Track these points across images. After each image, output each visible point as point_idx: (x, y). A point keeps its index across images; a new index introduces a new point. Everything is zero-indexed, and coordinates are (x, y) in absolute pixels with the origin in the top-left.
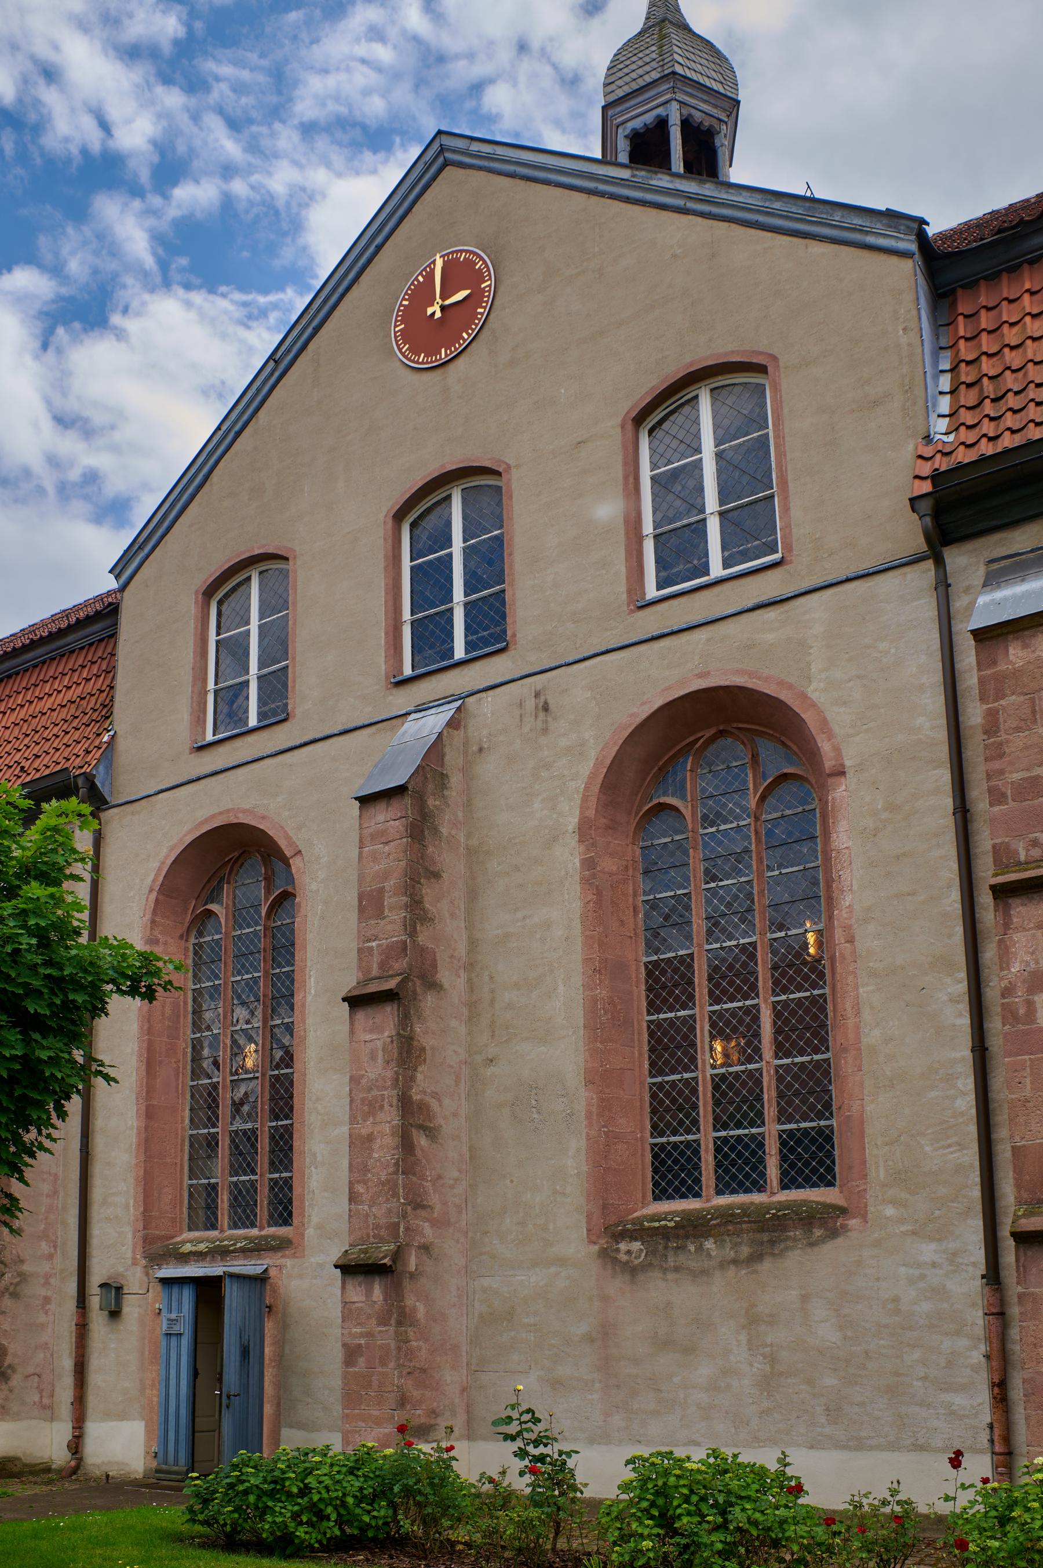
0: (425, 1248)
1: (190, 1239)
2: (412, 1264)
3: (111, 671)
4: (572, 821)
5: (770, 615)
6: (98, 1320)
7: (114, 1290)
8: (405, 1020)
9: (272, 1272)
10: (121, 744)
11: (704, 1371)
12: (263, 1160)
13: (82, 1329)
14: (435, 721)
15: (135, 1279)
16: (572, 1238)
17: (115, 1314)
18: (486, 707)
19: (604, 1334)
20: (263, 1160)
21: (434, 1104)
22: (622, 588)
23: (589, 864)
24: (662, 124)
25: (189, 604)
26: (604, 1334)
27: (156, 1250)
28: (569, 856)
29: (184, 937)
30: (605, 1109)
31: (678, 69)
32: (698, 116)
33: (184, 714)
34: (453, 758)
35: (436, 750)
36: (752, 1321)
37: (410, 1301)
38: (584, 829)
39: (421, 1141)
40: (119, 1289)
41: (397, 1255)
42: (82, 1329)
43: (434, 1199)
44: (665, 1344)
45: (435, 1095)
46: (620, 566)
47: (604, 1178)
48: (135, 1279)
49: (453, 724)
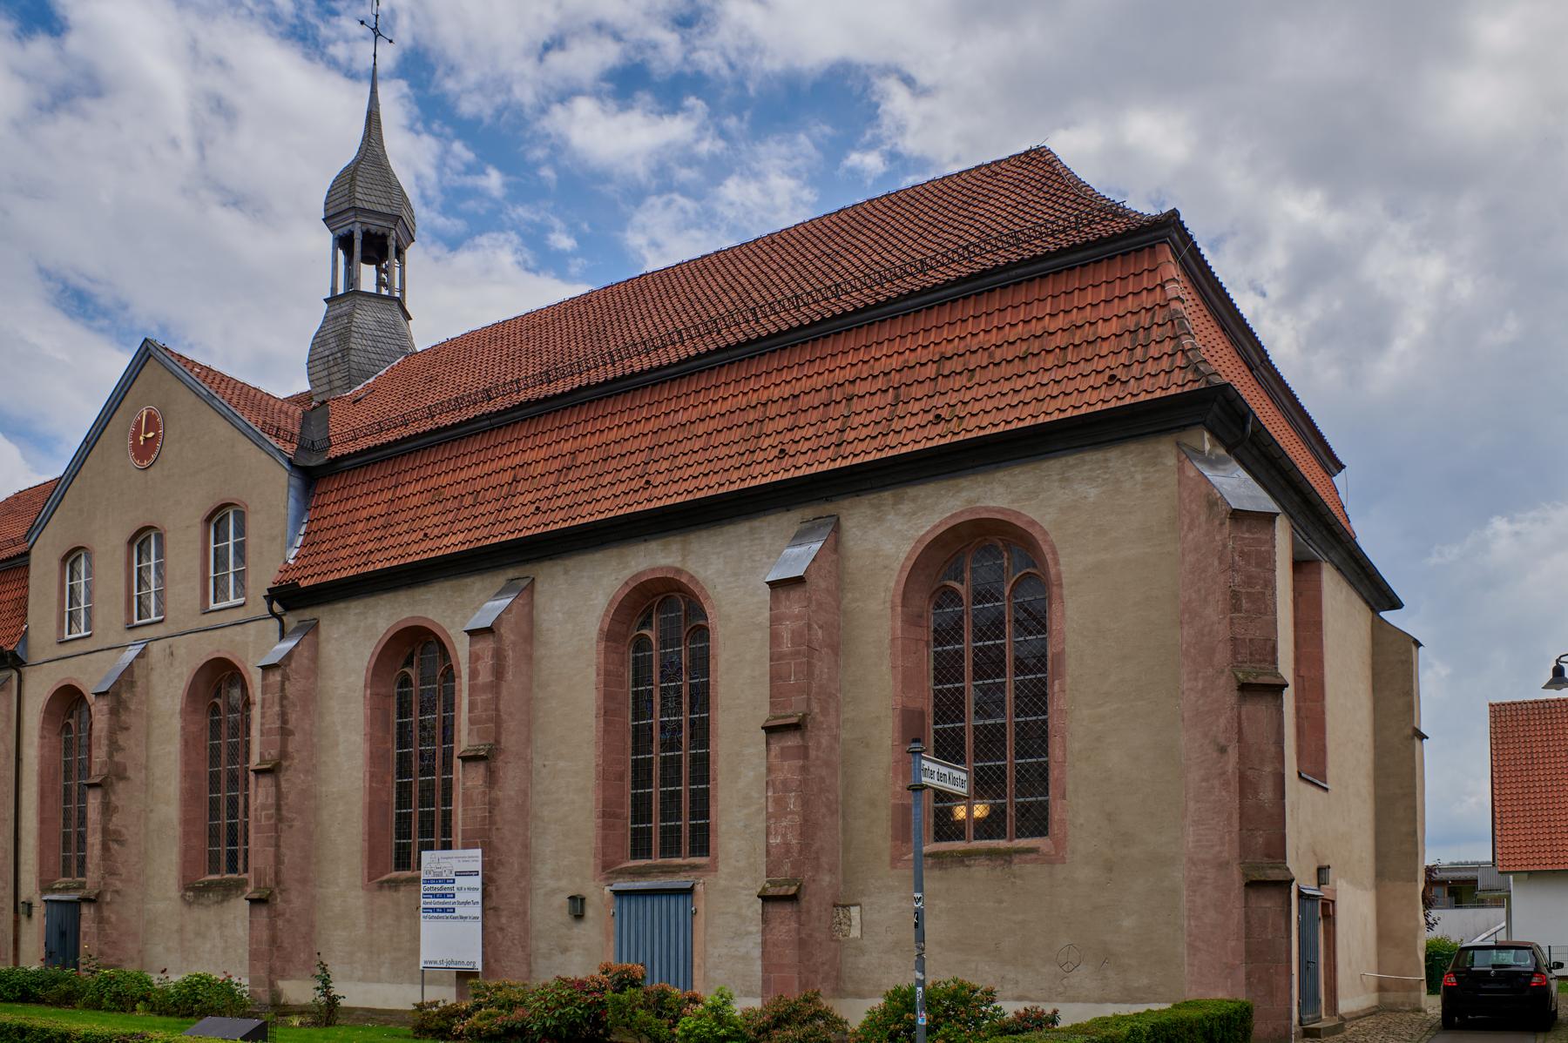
0: (117, 892)
1: (61, 882)
2: (108, 898)
3: (26, 587)
4: (178, 708)
5: (238, 628)
6: (23, 918)
7: (30, 905)
8: (105, 795)
9: (699, 888)
10: (31, 633)
11: (208, 946)
12: (416, 790)
13: (17, 923)
14: (131, 654)
15: (37, 901)
16: (174, 892)
17: (30, 916)
18: (155, 648)
19: (181, 930)
20: (416, 790)
21: (124, 830)
22: (198, 601)
23: (183, 728)
24: (351, 233)
25: (56, 564)
26: (181, 930)
27: (46, 886)
28: (176, 724)
29: (60, 734)
30: (186, 835)
31: (359, 204)
32: (373, 229)
33: (54, 623)
34: (137, 672)
35: (130, 668)
36: (222, 926)
37: (106, 913)
38: (183, 712)
39: (115, 846)
40: (583, 900)
41: (98, 895)
42: (17, 923)
43: (123, 871)
44: (198, 934)
45: (126, 827)
46: (198, 592)
47: (187, 863)
48: (37, 901)
49: (141, 655)
